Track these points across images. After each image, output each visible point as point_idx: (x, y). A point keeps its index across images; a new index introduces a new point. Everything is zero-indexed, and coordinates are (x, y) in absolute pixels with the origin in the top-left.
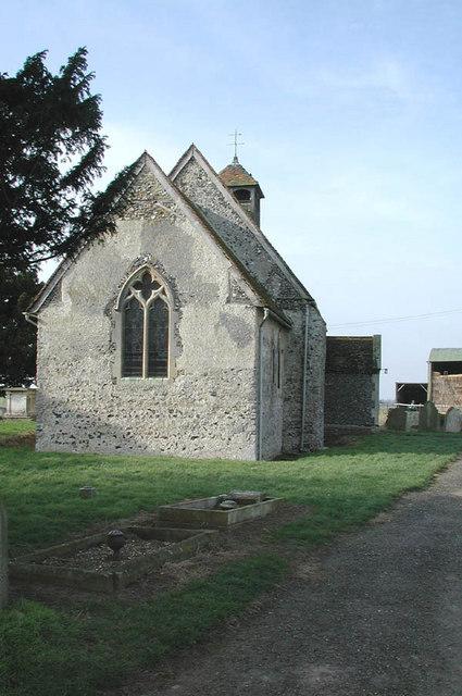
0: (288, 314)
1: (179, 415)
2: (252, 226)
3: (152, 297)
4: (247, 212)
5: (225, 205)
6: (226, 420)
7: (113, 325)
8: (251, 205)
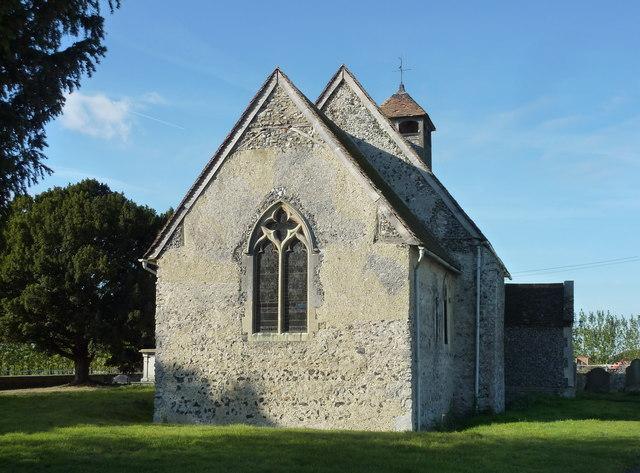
0: (459, 257)
1: (321, 376)
2: (416, 162)
3: (288, 237)
4: (413, 147)
5: (381, 133)
6: (376, 383)
7: (243, 271)
8: (418, 140)
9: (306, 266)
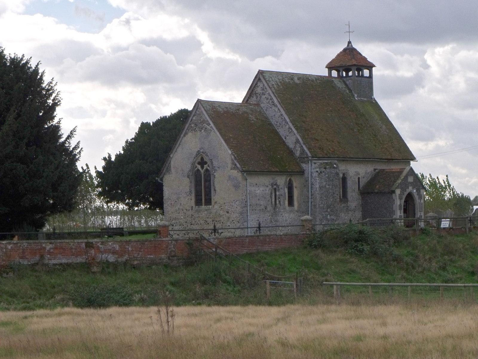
9: (210, 179)
